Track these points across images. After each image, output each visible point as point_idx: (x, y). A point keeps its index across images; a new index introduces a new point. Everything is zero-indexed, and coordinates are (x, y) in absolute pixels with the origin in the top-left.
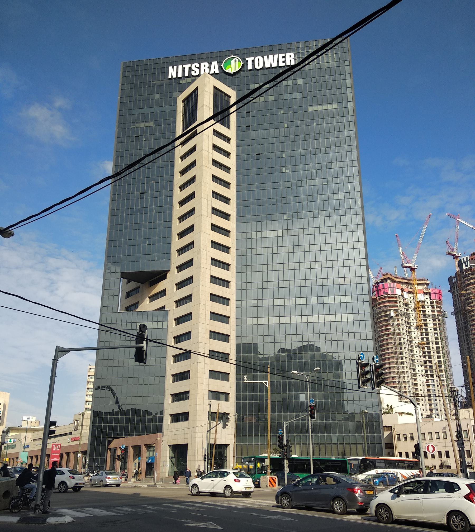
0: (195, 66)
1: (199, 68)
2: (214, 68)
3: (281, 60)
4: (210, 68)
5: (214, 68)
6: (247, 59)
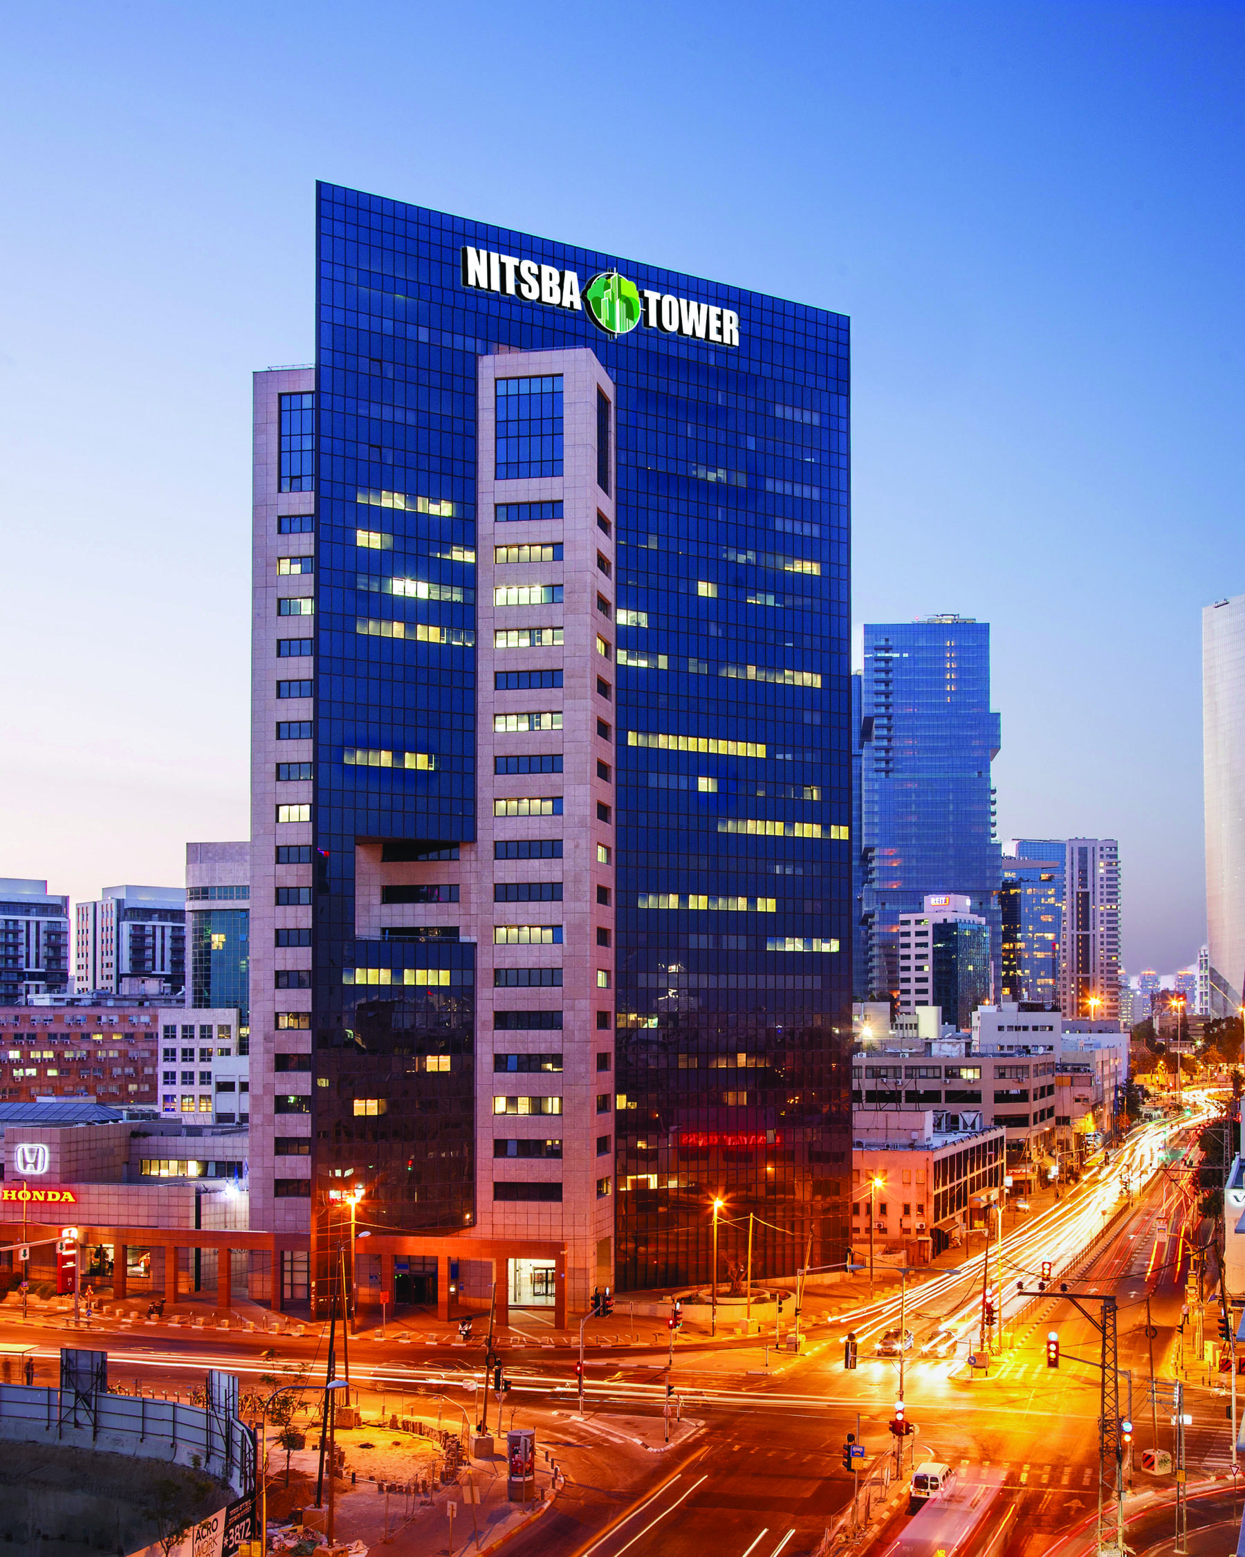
0: (529, 269)
1: (538, 278)
2: (571, 293)
3: (715, 323)
4: (561, 285)
5: (571, 293)
6: (647, 293)
